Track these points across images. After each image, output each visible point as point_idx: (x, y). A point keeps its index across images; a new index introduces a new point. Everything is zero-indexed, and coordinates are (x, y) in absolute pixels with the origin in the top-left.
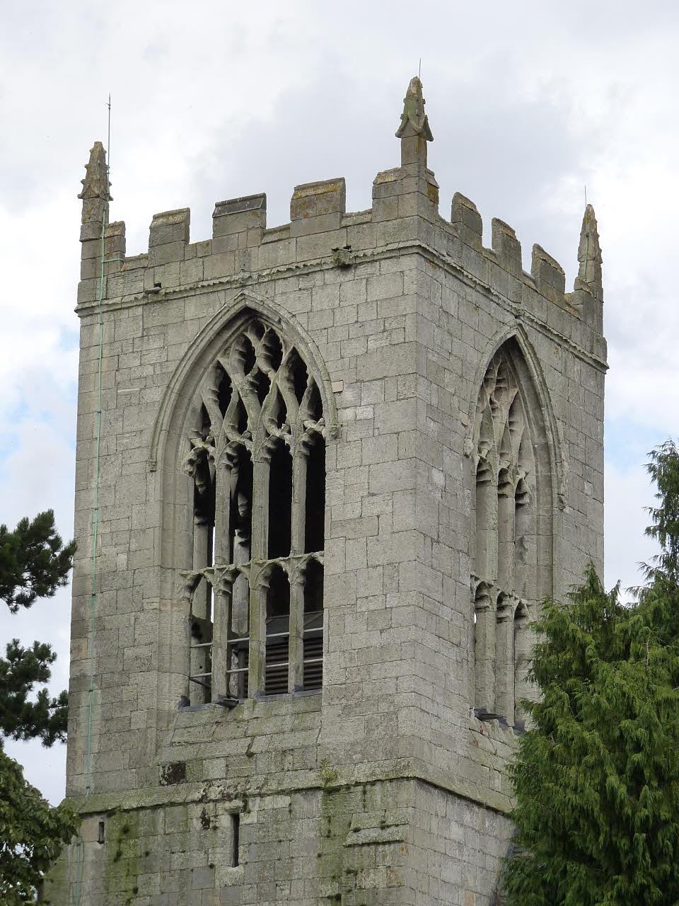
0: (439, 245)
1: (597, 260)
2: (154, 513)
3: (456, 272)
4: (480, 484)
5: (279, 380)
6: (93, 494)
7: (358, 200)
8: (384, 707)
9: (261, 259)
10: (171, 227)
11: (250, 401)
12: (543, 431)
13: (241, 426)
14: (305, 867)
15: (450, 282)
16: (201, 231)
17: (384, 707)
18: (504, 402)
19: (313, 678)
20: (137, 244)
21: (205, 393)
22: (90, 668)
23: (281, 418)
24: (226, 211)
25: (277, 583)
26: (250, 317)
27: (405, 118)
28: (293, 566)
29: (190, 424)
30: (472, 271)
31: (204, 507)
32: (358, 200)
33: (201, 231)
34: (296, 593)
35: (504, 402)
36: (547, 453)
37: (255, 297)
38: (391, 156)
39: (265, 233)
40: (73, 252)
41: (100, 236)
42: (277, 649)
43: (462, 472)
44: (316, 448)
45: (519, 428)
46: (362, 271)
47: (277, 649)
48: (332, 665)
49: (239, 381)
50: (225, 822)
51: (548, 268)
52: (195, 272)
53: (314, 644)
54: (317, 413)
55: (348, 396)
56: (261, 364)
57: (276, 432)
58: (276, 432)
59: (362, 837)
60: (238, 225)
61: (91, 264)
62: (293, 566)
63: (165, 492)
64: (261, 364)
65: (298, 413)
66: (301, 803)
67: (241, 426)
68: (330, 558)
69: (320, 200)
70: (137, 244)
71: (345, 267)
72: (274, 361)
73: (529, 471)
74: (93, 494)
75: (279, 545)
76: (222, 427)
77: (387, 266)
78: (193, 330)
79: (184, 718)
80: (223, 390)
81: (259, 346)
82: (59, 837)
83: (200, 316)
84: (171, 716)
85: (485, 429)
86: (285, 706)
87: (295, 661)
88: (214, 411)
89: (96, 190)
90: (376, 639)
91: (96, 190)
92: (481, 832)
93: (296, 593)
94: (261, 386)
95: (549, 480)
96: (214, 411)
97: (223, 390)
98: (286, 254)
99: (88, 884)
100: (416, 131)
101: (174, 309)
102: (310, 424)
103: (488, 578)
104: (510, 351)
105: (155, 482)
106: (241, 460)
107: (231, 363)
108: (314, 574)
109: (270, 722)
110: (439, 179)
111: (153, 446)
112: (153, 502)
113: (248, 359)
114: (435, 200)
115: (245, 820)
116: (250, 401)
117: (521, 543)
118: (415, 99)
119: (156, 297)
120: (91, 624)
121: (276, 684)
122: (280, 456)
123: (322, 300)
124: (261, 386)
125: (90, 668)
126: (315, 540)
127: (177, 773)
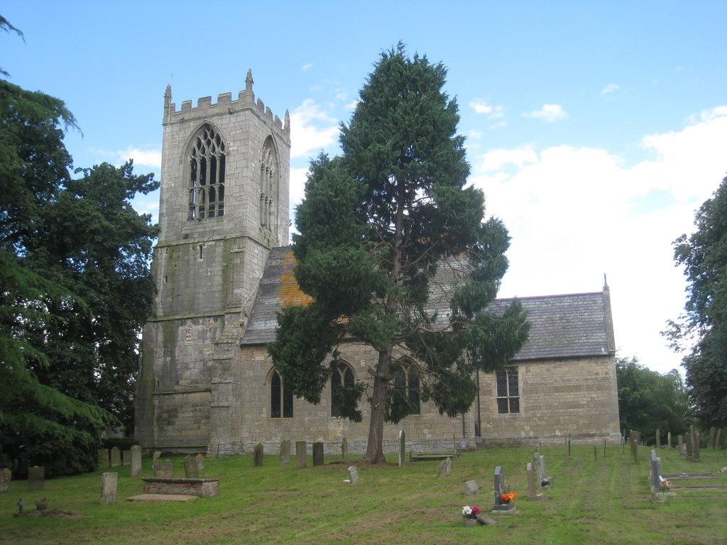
0: (255, 109)
1: (289, 122)
2: (181, 173)
3: (258, 116)
4: (262, 170)
5: (214, 141)
6: (166, 169)
7: (235, 98)
8: (239, 220)
9: (210, 112)
10: (187, 105)
11: (206, 146)
12: (276, 159)
13: (203, 152)
14: (219, 259)
15: (256, 118)
16: (195, 105)
17: (239, 220)
18: (269, 150)
19: (221, 213)
20: (178, 109)
21: (195, 144)
22: (164, 211)
23: (214, 150)
24: (201, 100)
25: (212, 191)
26: (207, 127)
27: (247, 78)
28: (216, 187)
29: (191, 152)
30: (262, 117)
31: (193, 177)
32: (235, 98)
33: (195, 105)
34: (217, 193)
35: (269, 150)
36: (277, 165)
37: (208, 120)
38: (243, 87)
39: (211, 105)
40: (162, 110)
41: (169, 107)
42: (212, 207)
43: (259, 165)
44: (223, 159)
45: (271, 158)
46: (236, 114)
47: (212, 207)
48: (225, 210)
49: (203, 141)
50: (198, 248)
51: (278, 122)
52: (193, 115)
53: (221, 206)
54: (223, 148)
55: (231, 144)
56: (209, 137)
57: (212, 154)
58: (212, 154)
59: (233, 251)
60: (205, 105)
61: (167, 113)
62: (216, 187)
63: (184, 168)
64: (209, 137)
65: (218, 149)
66: (218, 244)
67: (203, 152)
68: (227, 184)
69: (225, 98)
70: (178, 109)
71: (231, 113)
72: (212, 137)
73: (273, 168)
74: (166, 169)
75: (213, 181)
76: (199, 153)
77: (241, 113)
78: (192, 129)
79: (188, 223)
80: (199, 144)
81: (208, 133)
82: (474, 240)
83: (193, 126)
84: (185, 223)
85: (264, 157)
86: (213, 220)
87: (217, 209)
88: (197, 149)
89: (168, 96)
90: (237, 203)
91: (168, 96)
92: (262, 252)
93: (217, 193)
94: (209, 143)
95: (278, 171)
96: (197, 149)
97: (199, 144)
98: (217, 110)
99: (163, 264)
100: (250, 82)
101: (186, 125)
102: (221, 152)
103: (264, 192)
104: (269, 138)
105: (182, 166)
106: (203, 162)
107: (201, 137)
108: (222, 189)
109: (209, 223)
110: (255, 94)
111: (181, 157)
112: (183, 171)
113: (206, 137)
114: (254, 99)
115: (204, 247)
116: (206, 146)
117: (271, 186)
118: (249, 74)
119: (183, 121)
120: (165, 200)
121: (211, 215)
122: (213, 160)
123: (225, 121)
124: (209, 143)
125: (164, 211)
126: (222, 179)
127: (186, 237)
